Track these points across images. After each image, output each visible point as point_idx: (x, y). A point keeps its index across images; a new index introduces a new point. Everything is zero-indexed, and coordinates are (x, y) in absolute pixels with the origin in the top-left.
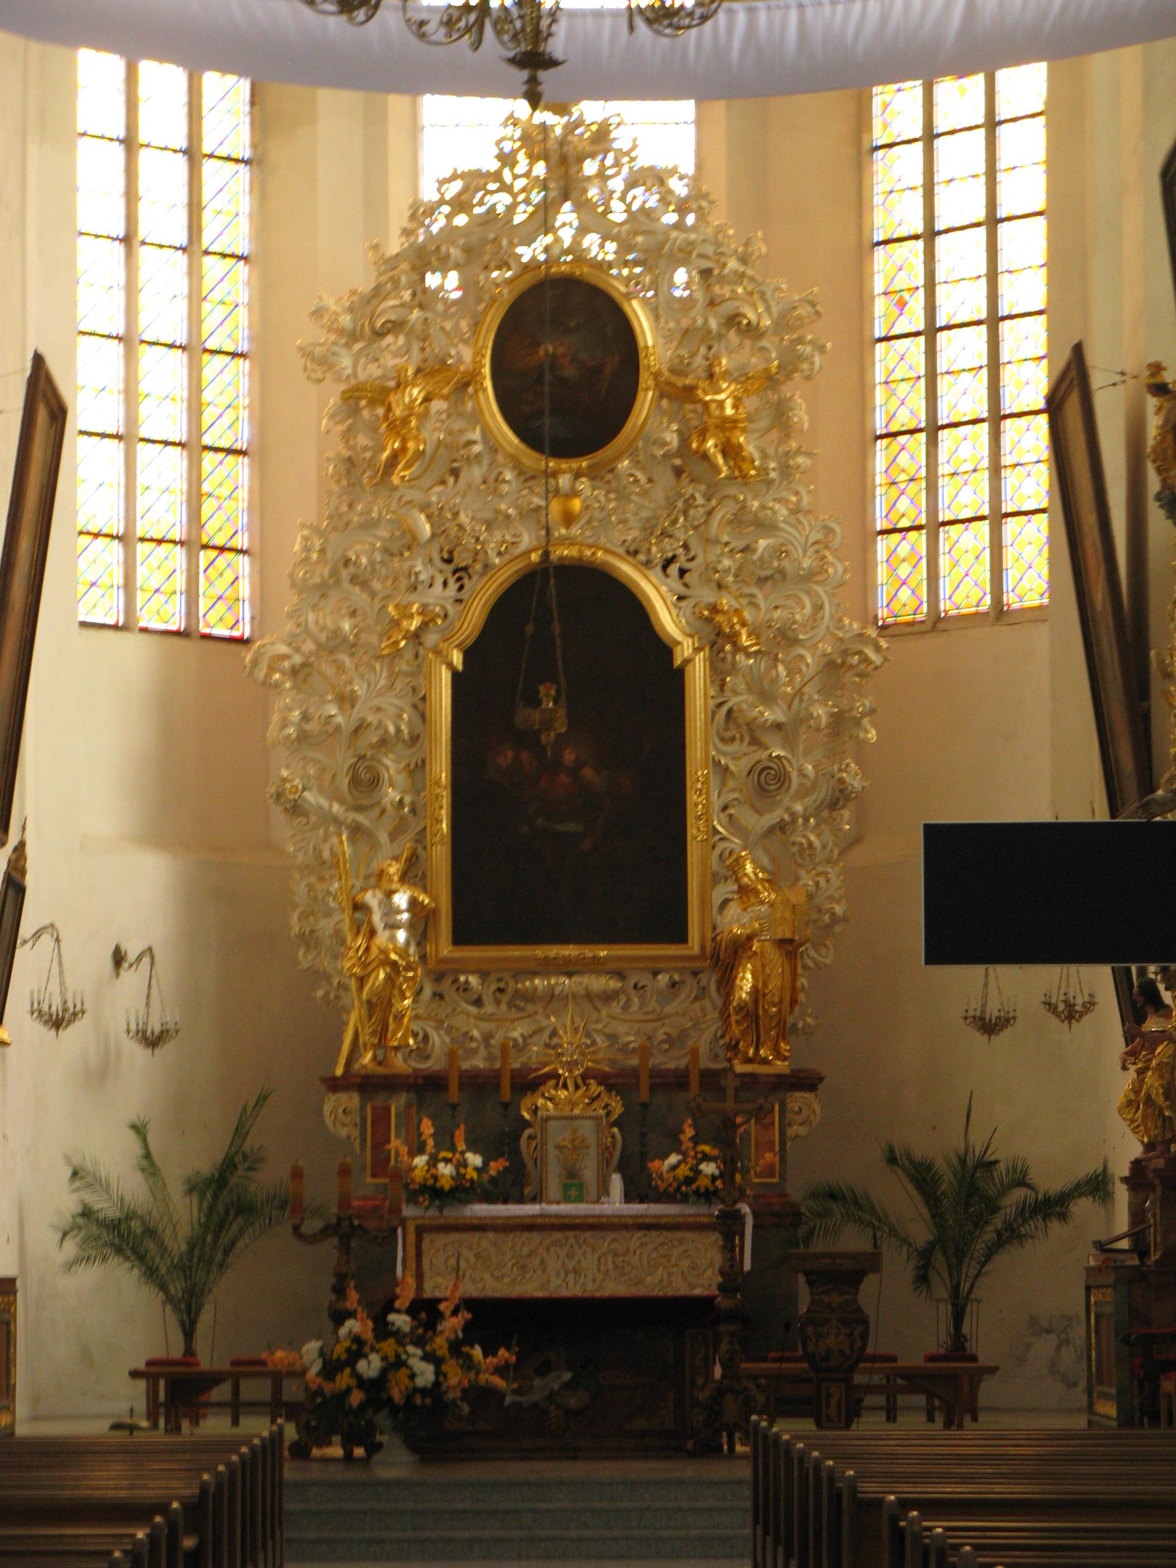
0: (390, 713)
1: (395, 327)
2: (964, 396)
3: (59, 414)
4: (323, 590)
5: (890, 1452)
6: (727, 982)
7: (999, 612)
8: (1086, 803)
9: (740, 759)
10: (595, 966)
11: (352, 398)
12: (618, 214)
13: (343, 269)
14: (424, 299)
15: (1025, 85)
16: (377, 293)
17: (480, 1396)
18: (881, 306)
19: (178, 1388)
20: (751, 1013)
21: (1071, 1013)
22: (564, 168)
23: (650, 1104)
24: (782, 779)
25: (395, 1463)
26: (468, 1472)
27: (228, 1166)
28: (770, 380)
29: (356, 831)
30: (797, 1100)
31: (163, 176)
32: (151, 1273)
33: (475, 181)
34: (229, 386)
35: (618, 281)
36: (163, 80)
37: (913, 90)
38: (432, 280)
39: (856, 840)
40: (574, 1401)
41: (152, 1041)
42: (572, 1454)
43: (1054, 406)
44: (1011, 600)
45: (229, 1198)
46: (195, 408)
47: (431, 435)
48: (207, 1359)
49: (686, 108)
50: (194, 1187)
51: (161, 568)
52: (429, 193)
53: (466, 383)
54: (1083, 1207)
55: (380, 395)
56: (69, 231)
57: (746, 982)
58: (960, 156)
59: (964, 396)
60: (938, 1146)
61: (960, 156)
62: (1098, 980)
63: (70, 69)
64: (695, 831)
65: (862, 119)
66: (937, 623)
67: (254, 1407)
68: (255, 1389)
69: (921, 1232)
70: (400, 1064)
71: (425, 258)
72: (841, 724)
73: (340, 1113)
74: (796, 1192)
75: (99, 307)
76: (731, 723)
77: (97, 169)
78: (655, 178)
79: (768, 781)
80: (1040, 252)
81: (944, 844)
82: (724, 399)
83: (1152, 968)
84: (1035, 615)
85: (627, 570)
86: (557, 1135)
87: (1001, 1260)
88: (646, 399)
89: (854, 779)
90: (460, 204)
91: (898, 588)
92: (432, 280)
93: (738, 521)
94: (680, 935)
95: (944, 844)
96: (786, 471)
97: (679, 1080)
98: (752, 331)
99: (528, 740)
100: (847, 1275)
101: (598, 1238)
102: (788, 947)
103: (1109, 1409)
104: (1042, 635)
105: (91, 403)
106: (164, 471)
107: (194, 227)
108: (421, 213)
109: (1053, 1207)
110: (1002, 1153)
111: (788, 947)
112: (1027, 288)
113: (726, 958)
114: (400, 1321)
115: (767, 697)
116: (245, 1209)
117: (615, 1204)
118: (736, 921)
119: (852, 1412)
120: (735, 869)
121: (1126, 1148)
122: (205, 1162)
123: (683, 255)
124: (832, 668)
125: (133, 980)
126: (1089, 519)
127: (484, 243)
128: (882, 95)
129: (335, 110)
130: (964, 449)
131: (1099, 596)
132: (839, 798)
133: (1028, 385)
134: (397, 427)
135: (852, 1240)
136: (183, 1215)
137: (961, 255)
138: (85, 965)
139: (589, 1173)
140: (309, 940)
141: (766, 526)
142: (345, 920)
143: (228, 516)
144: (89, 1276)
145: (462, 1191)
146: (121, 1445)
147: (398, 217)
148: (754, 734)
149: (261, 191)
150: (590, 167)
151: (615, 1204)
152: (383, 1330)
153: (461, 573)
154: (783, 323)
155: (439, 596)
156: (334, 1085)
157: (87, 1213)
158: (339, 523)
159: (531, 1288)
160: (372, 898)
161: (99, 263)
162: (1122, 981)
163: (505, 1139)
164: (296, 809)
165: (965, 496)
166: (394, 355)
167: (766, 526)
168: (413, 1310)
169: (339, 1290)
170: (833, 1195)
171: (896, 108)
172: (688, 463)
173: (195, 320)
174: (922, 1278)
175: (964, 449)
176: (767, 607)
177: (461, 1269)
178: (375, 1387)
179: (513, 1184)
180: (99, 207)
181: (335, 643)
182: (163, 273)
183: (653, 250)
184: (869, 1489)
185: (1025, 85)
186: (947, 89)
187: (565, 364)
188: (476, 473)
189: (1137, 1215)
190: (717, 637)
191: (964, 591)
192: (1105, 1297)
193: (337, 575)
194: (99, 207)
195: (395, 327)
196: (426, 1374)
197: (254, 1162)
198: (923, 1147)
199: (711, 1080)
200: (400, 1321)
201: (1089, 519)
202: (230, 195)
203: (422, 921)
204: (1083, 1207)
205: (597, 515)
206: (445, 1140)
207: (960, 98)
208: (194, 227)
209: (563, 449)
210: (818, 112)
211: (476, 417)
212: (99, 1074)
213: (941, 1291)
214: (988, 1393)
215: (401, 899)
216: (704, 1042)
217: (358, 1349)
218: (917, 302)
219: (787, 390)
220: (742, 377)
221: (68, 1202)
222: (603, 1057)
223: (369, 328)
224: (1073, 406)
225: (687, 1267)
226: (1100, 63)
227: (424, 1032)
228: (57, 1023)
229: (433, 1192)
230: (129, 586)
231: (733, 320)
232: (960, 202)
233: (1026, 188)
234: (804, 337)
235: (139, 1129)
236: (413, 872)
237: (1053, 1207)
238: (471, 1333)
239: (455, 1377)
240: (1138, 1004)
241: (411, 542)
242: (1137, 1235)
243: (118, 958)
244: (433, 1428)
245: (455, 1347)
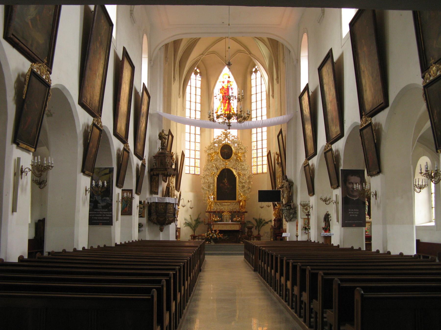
0: (211, 180)
1: (212, 149)
2: (260, 155)
3: (184, 156)
4: (206, 170)
5: (254, 242)
6: (240, 204)
7: (263, 173)
8: (270, 189)
9: (241, 185)
10: (229, 202)
11: (208, 154)
12: (231, 139)
13: (208, 144)
14: (214, 146)
15: (265, 129)
16: (211, 146)
17: (220, 238)
18: (253, 147)
19: (194, 237)
20: (242, 206)
21: (269, 207)
22: (226, 135)
23: (233, 214)
24: (244, 187)
25: (213, 243)
26: (220, 244)
27: (198, 219)
28: (244, 153)
29: (208, 191)
30: (245, 214)
31: (193, 136)
32: (191, 228)
33: (219, 136)
34: (198, 153)
35: (231, 145)
36: (193, 128)
37: (255, 129)
38: (215, 145)
39: (250, 192)
40: (228, 238)
41: (191, 208)
42: (228, 243)
43: (268, 156)
44: (264, 172)
45: (198, 221)
46: (195, 155)
47: (215, 157)
48: (196, 235)
49: (236, 130)
50: (195, 220)
51: (192, 169)
52: (215, 138)
53: (218, 153)
54: (269, 223)
55: (211, 154)
56: (184, 140)
57: (241, 204)
58: (259, 135)
59: (260, 155)
60: (257, 217)
61: (259, 135)
62: (271, 203)
63: (185, 127)
64: (237, 191)
65: (251, 132)
66: (257, 174)
67: (200, 239)
68: (200, 237)
69: (256, 225)
70: (212, 210)
71: (214, 143)
72: (249, 182)
73: (207, 214)
74: (245, 221)
75: (187, 147)
76: (240, 182)
77: (187, 135)
78: (234, 136)
79: (243, 187)
80: (266, 143)
81: (260, 192)
82: (240, 155)
83: (276, 203)
84: (266, 173)
85: (231, 169)
86: (225, 216)
87: (263, 227)
88: (233, 155)
89: (250, 187)
90: (218, 138)
91: (254, 171)
92: (215, 145)
93: (241, 165)
94: (236, 200)
95: (260, 192)
96: (245, 161)
97: (236, 212)
98: (242, 149)
99: (224, 183)
100: (250, 228)
101: (229, 225)
102: (245, 201)
103: (272, 239)
104: (266, 175)
105: (187, 155)
106: (192, 161)
107: (195, 140)
108: (214, 139)
109: (267, 223)
110: (263, 218)
111: (245, 201)
112: (265, 145)
113: (239, 202)
114: (213, 232)
115: (243, 180)
116: (199, 222)
117: (230, 222)
118: (240, 199)
119: (250, 240)
120: (240, 194)
121: (274, 218)
122: (196, 218)
123: (236, 143)
124: (249, 177)
125: (190, 203)
126: (271, 165)
127: (220, 142)
128: (253, 129)
129: (207, 130)
130: (260, 159)
131: (271, 171)
132: (249, 188)
133: (265, 154)
134: (212, 157)
135: (250, 225)
136: (194, 223)
137: (259, 143)
138: (186, 202)
139: (228, 220)
140: (204, 200)
141: (243, 165)
142: (207, 198)
143: (198, 164)
144: (186, 228)
145: (217, 221)
146: (189, 241)
147: (212, 139)
148: (242, 183)
149: (201, 137)
150: (228, 135)
151: (230, 222)
152: (212, 232)
153: (218, 169)
154: (244, 148)
155: (216, 171)
156: (207, 212)
157: (186, 223)
158: (207, 165)
159: (223, 229)
160: (210, 196)
161: (187, 144)
162: (273, 203)
163: (221, 217)
164: (203, 189)
165: (260, 163)
166: (212, 151)
167: (243, 165)
168: (215, 231)
169: (208, 229)
170: (250, 222)
171: (254, 131)
172: (237, 160)
173: (195, 148)
174: (256, 229)
175: (260, 159)
176: (243, 172)
177: (216, 227)
178: (211, 237)
179: (222, 221)
180: (187, 138)
181: (207, 175)
182: (193, 144)
183: (234, 142)
184: (256, 245)
185: (265, 129)
186: (258, 129)
187: (226, 152)
188: (219, 161)
189: (275, 223)
190: (239, 175)
191: (260, 171)
192: (272, 230)
193: (207, 169)
194: (187, 138)
195: (212, 149)
196: (215, 236)
197: (200, 218)
198: (256, 218)
199: (238, 212)
200: (213, 232)
201: (271, 165)
202: (198, 137)
203: (214, 198)
204: (269, 223)
205: (229, 164)
206: (216, 217)
207: (259, 130)
208: (195, 140)
209: (227, 159)
210: (247, 131)
211: (219, 156)
212: (187, 211)
213: (257, 229)
214: (262, 238)
215: (212, 197)
216: (238, 209)
217: (210, 234)
218: (256, 147)
219: (43, 173)
220: (241, 153)
221: (184, 222)
222: (229, 210)
223: (210, 149)
224: (269, 156)
225: (237, 227)
226: (271, 127)
227: (214, 208)
228: (183, 207)
229: (215, 221)
230: (189, 170)
231: (240, 148)
232: (259, 138)
233: (265, 137)
234: (247, 150)
235: (190, 216)
236: (213, 194)
237: (267, 223)
238: (219, 233)
239: (218, 236)
240: (274, 206)
241: (213, 166)
242: (275, 225)
243: (188, 201)
244: (216, 241)
245: (218, 234)
